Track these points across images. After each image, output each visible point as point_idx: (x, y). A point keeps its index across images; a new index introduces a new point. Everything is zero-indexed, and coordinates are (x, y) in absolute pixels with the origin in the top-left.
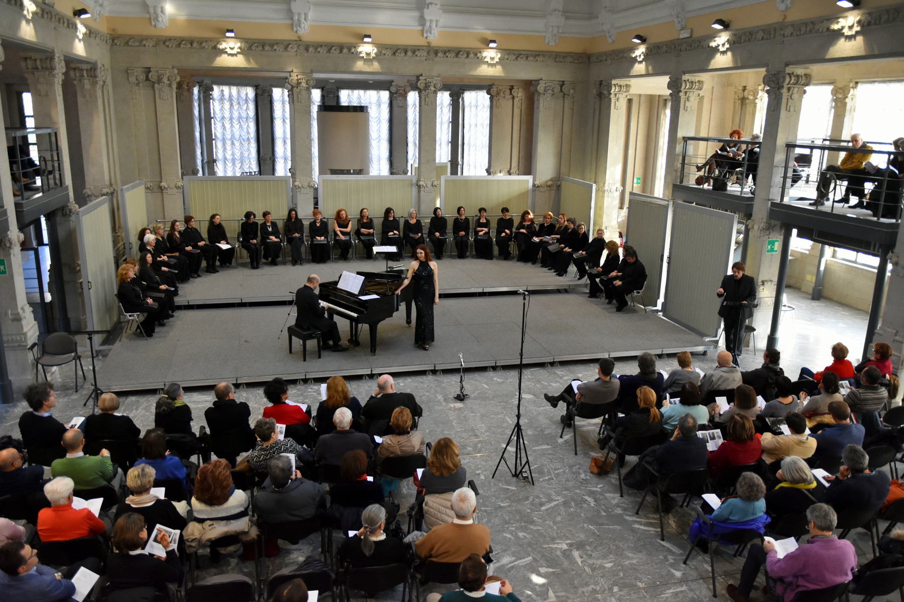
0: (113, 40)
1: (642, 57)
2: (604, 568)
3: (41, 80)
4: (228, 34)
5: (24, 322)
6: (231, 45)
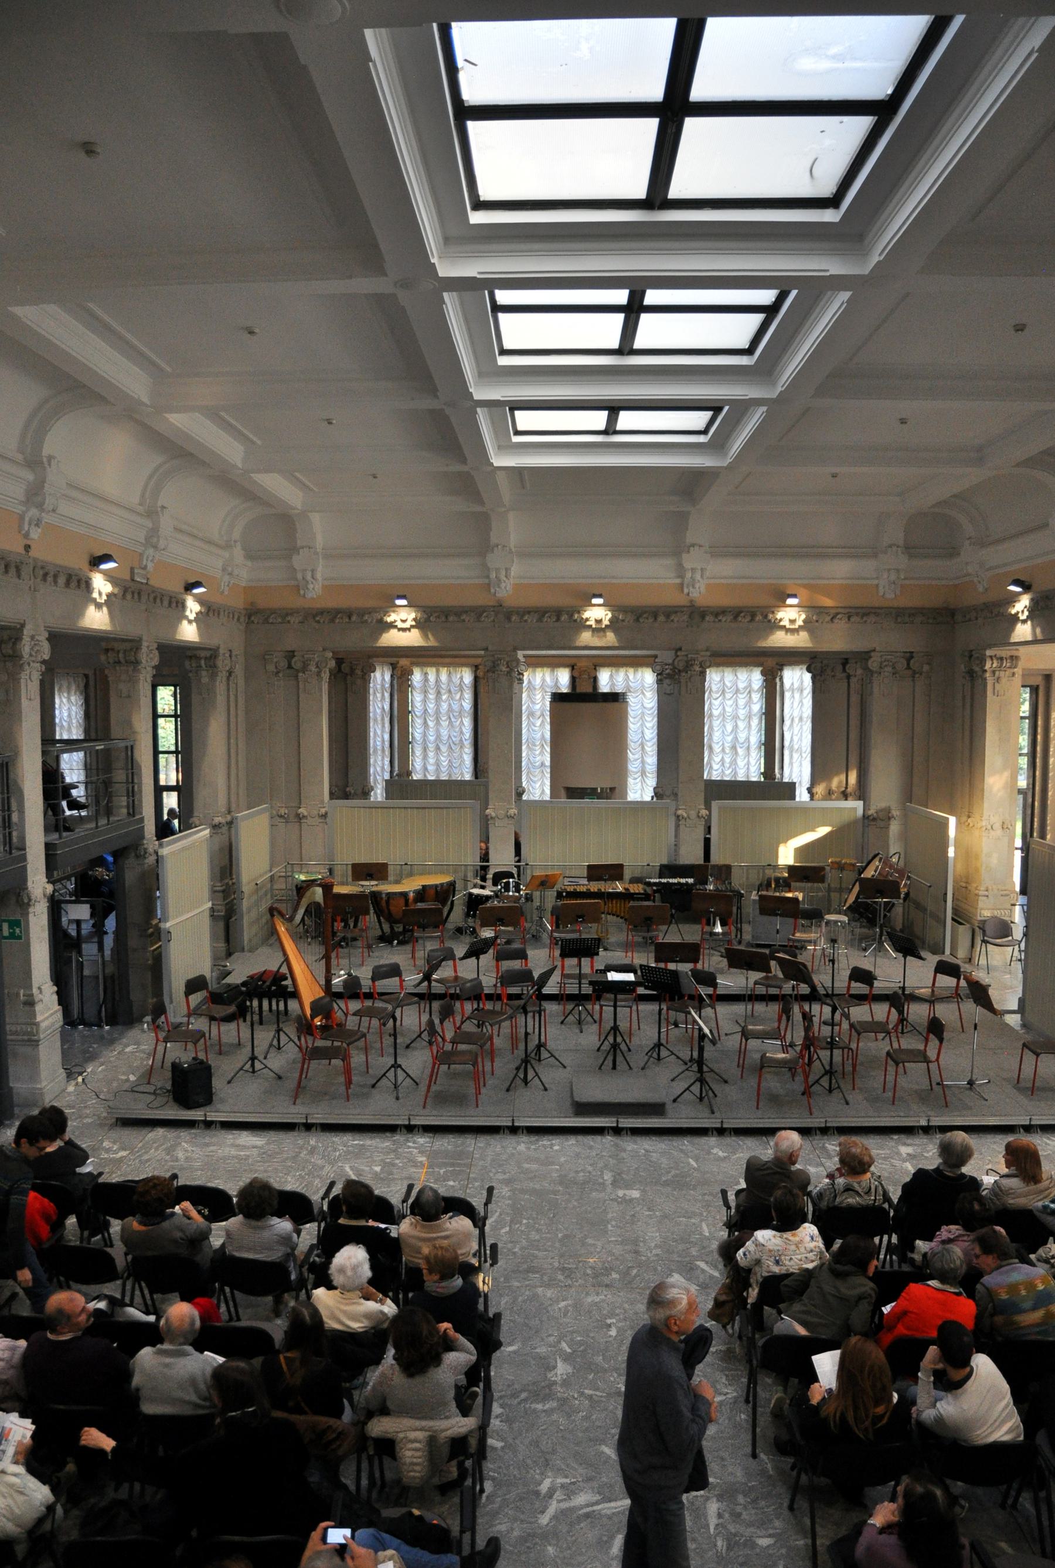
0: (249, 618)
1: (1026, 613)
2: (754, 1545)
3: (124, 677)
4: (399, 602)
5: (38, 1008)
6: (403, 615)
